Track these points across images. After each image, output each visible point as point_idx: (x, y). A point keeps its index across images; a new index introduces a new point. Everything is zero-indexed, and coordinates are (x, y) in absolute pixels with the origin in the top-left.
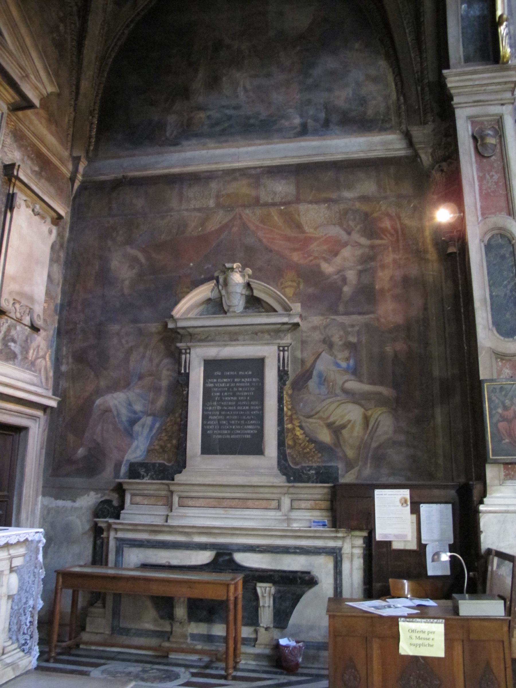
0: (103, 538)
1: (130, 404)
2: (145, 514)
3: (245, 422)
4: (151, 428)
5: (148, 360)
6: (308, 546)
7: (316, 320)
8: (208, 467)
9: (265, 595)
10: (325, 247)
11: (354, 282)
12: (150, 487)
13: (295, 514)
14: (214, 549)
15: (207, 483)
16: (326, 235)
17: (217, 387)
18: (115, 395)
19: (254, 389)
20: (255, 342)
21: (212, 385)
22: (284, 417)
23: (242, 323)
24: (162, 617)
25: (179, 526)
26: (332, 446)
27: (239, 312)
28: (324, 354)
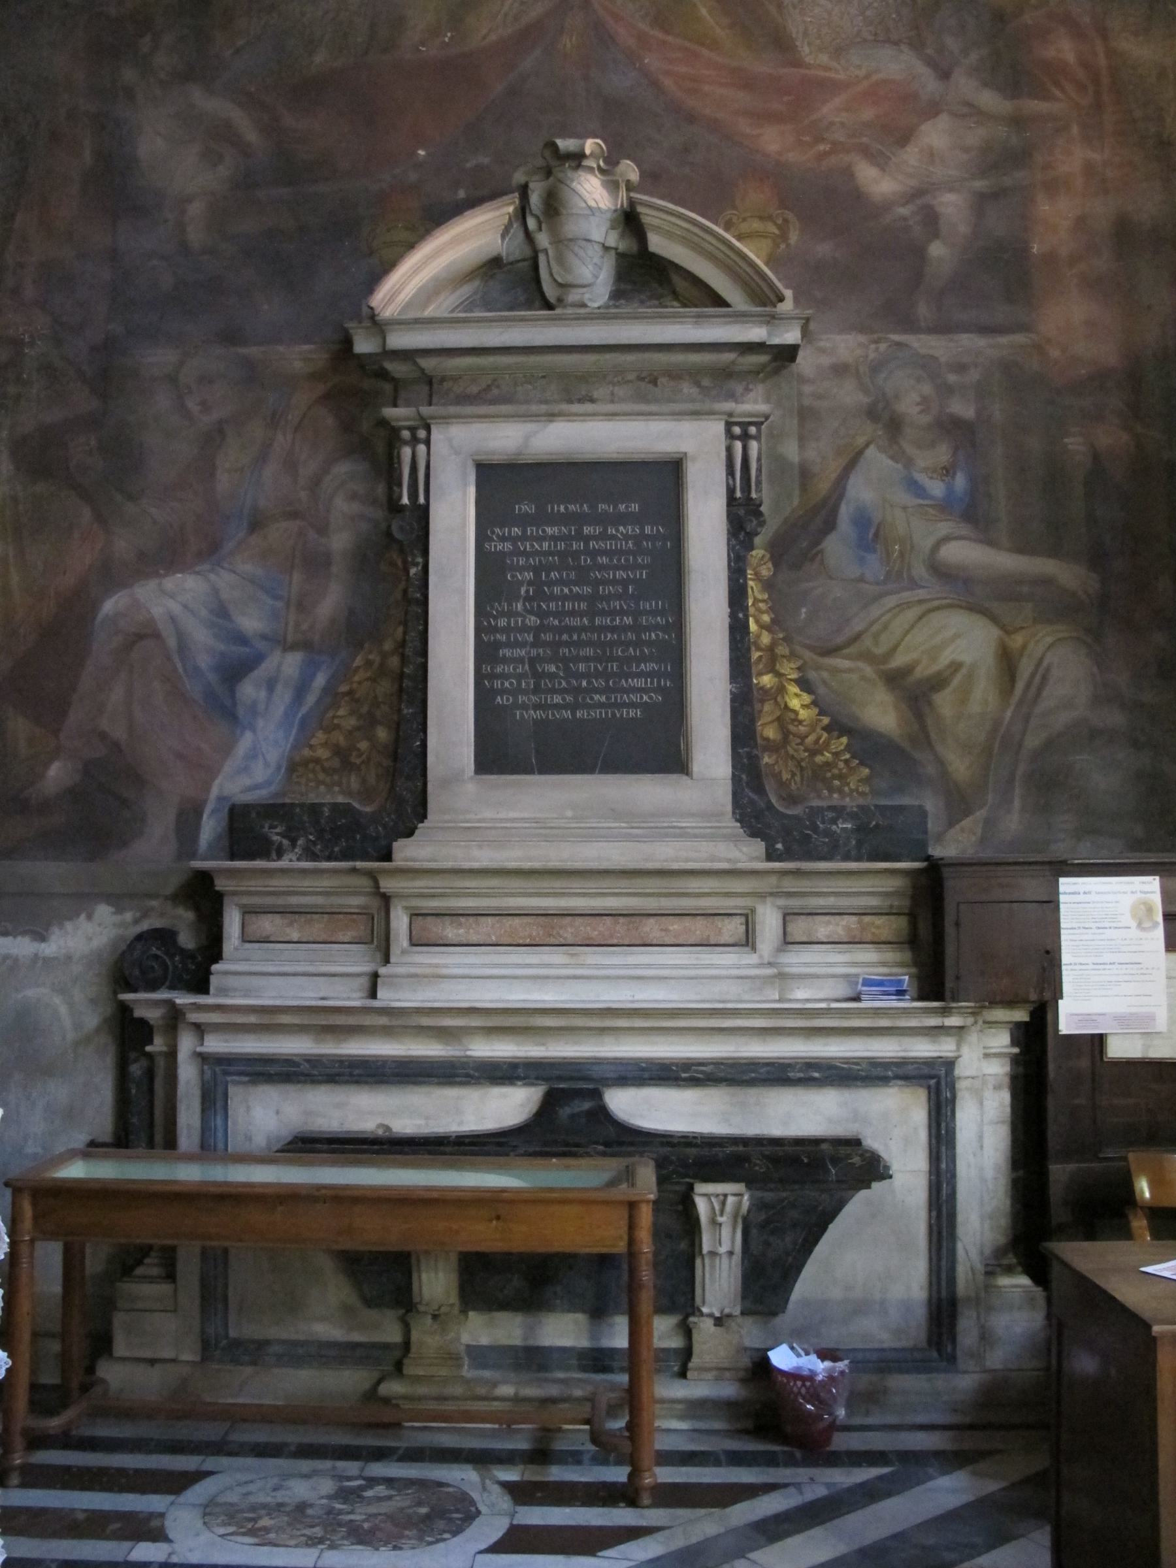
0: (150, 1056)
1: (221, 611)
2: (295, 975)
3: (620, 667)
4: (300, 691)
5: (284, 466)
6: (847, 1060)
7: (845, 345)
8: (501, 816)
9: (720, 1219)
10: (868, 114)
11: (963, 229)
12: (307, 883)
13: (798, 960)
14: (537, 1078)
15: (512, 865)
16: (867, 76)
17: (524, 553)
18: (170, 583)
19: (648, 560)
20: (653, 408)
21: (508, 546)
22: (749, 650)
23: (612, 342)
24: (369, 1302)
25: (419, 1011)
26: (906, 745)
27: (596, 305)
28: (871, 451)
